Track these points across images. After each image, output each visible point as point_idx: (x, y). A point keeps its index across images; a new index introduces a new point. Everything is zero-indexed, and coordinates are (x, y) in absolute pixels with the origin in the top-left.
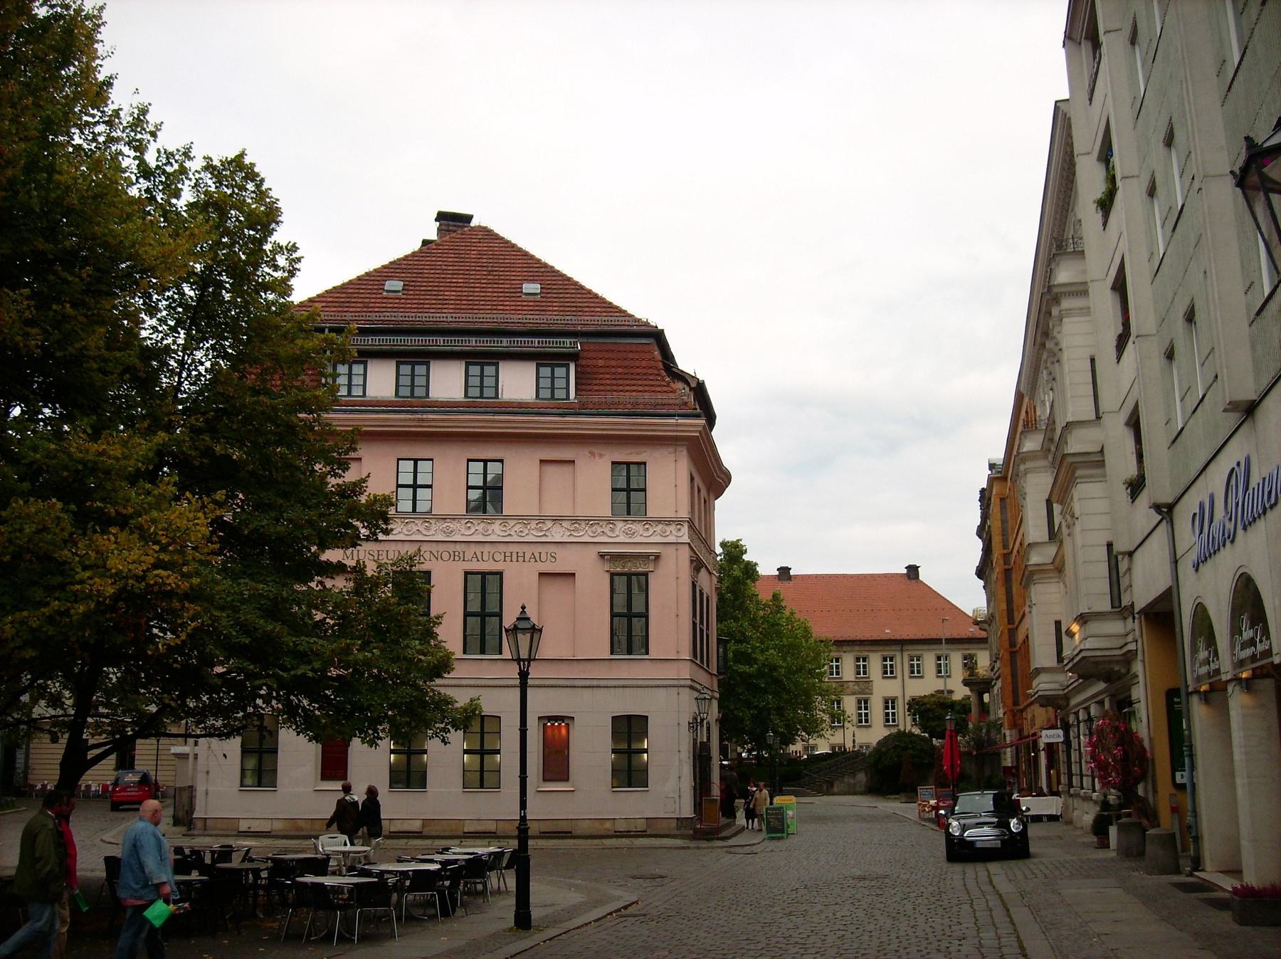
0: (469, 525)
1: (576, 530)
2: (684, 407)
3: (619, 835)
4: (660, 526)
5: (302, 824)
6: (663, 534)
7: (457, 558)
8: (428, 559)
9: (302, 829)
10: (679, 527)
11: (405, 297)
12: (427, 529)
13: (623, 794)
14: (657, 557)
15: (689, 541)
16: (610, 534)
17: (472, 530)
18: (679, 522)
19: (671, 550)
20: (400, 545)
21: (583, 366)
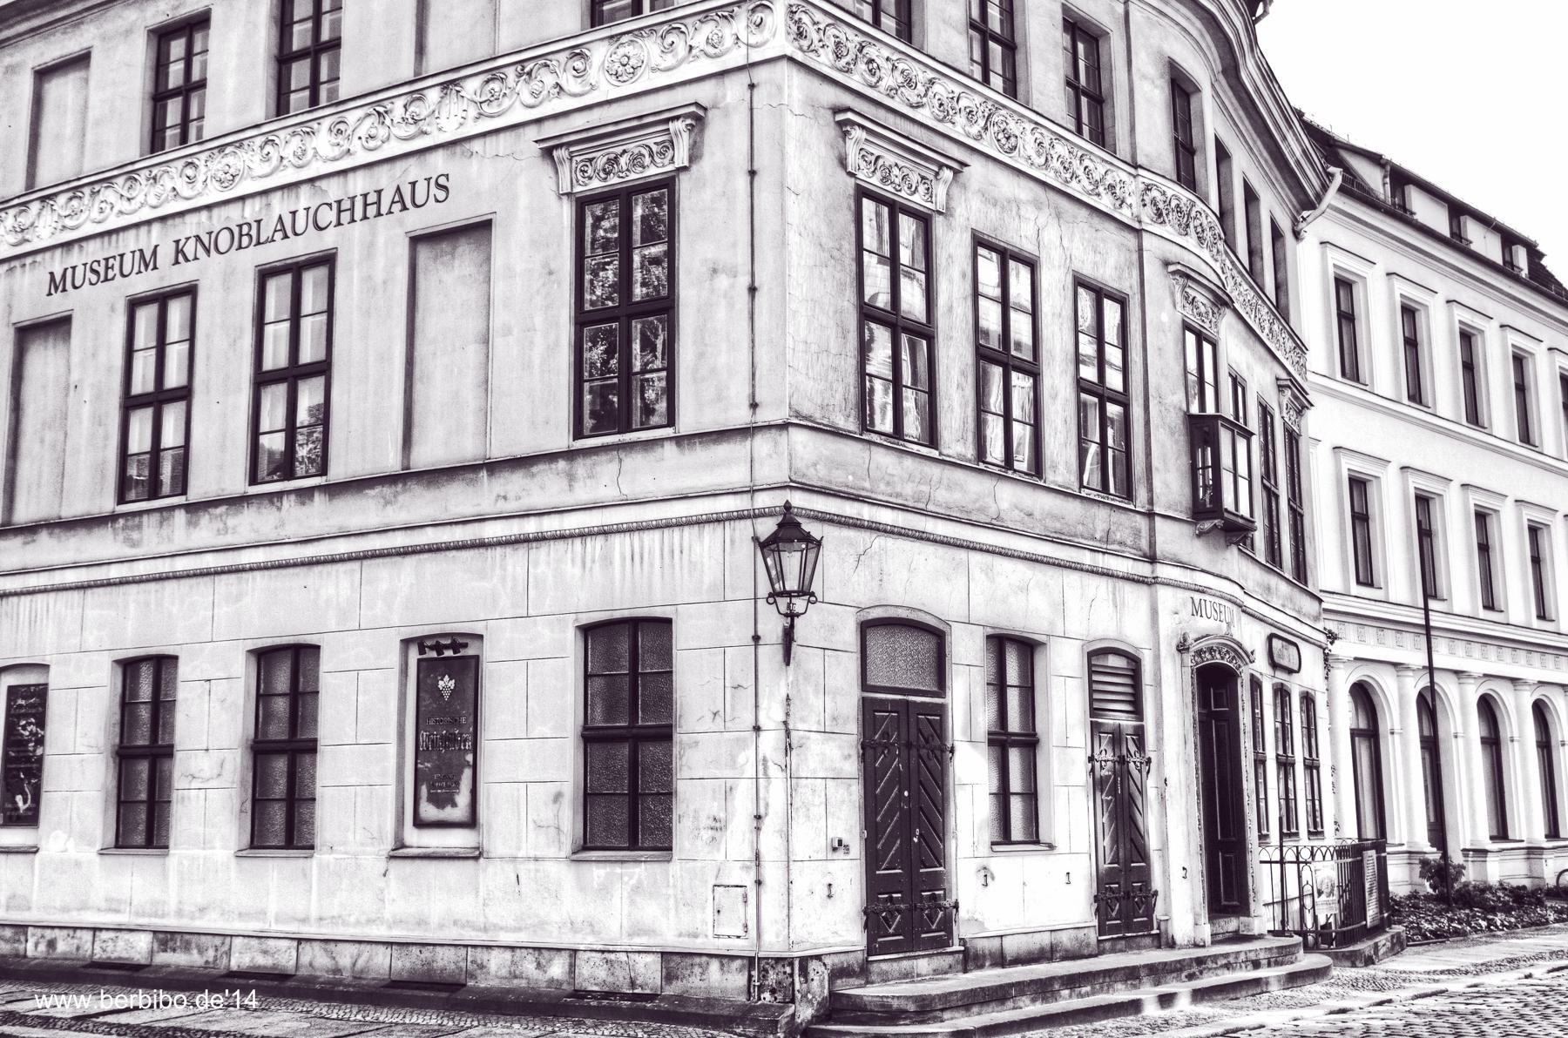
7: (245, 240)
8: (191, 257)
19: (734, 89)
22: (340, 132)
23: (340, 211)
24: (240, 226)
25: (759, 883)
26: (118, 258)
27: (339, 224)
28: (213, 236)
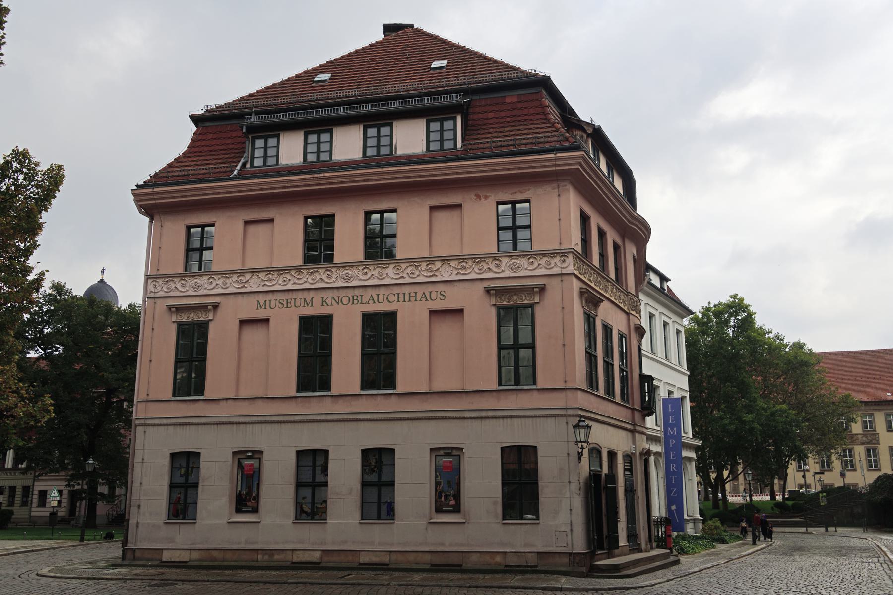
1: (464, 268)
4: (545, 259)
5: (216, 554)
6: (548, 266)
7: (355, 302)
8: (329, 304)
9: (216, 560)
10: (563, 258)
13: (513, 527)
19: (556, 281)
20: (305, 293)
21: (474, 120)
23: (398, 297)
24: (353, 296)
27: (398, 301)
28: (340, 298)
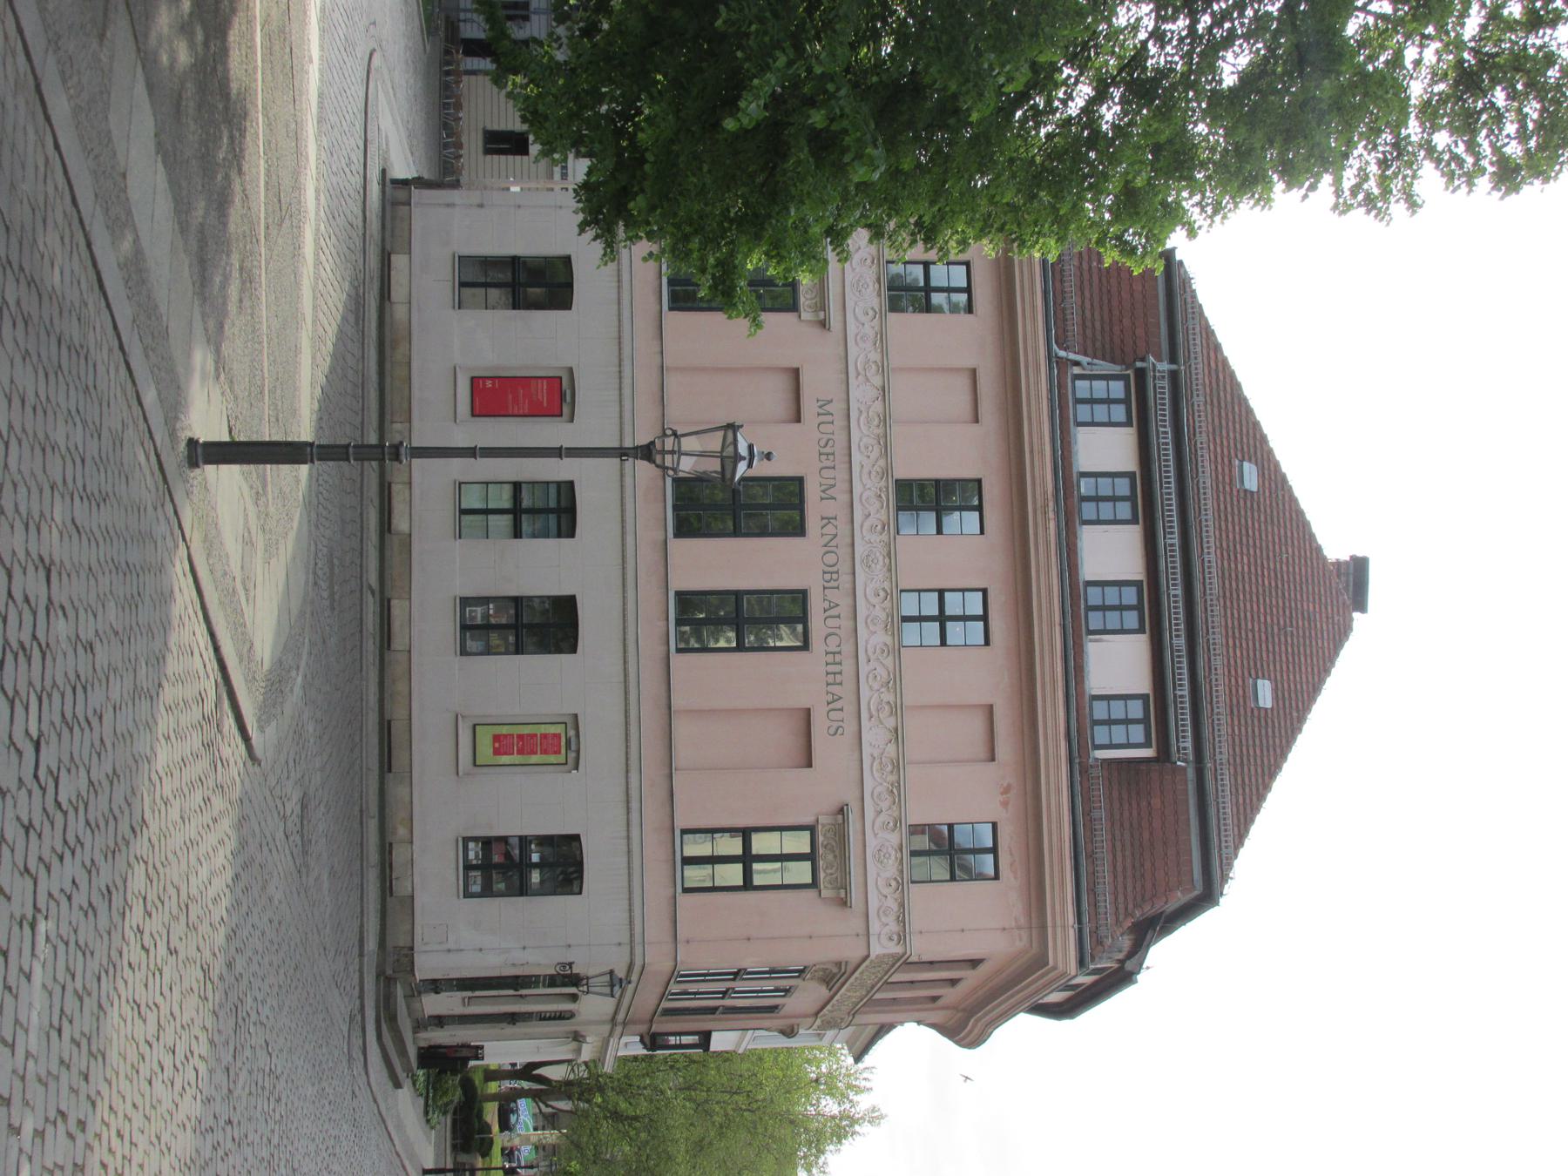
0: (882, 594)
2: (1094, 939)
3: (386, 849)
4: (895, 907)
7: (828, 577)
8: (825, 531)
10: (895, 937)
11: (1235, 493)
12: (872, 529)
14: (844, 903)
15: (873, 956)
16: (867, 525)
17: (863, 318)
18: (902, 938)
19: (856, 924)
22: (883, 651)
23: (834, 653)
24: (837, 572)
25: (449, 951)
26: (832, 464)
